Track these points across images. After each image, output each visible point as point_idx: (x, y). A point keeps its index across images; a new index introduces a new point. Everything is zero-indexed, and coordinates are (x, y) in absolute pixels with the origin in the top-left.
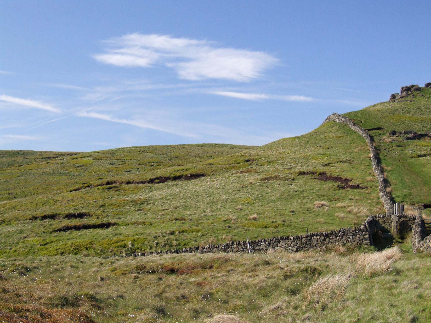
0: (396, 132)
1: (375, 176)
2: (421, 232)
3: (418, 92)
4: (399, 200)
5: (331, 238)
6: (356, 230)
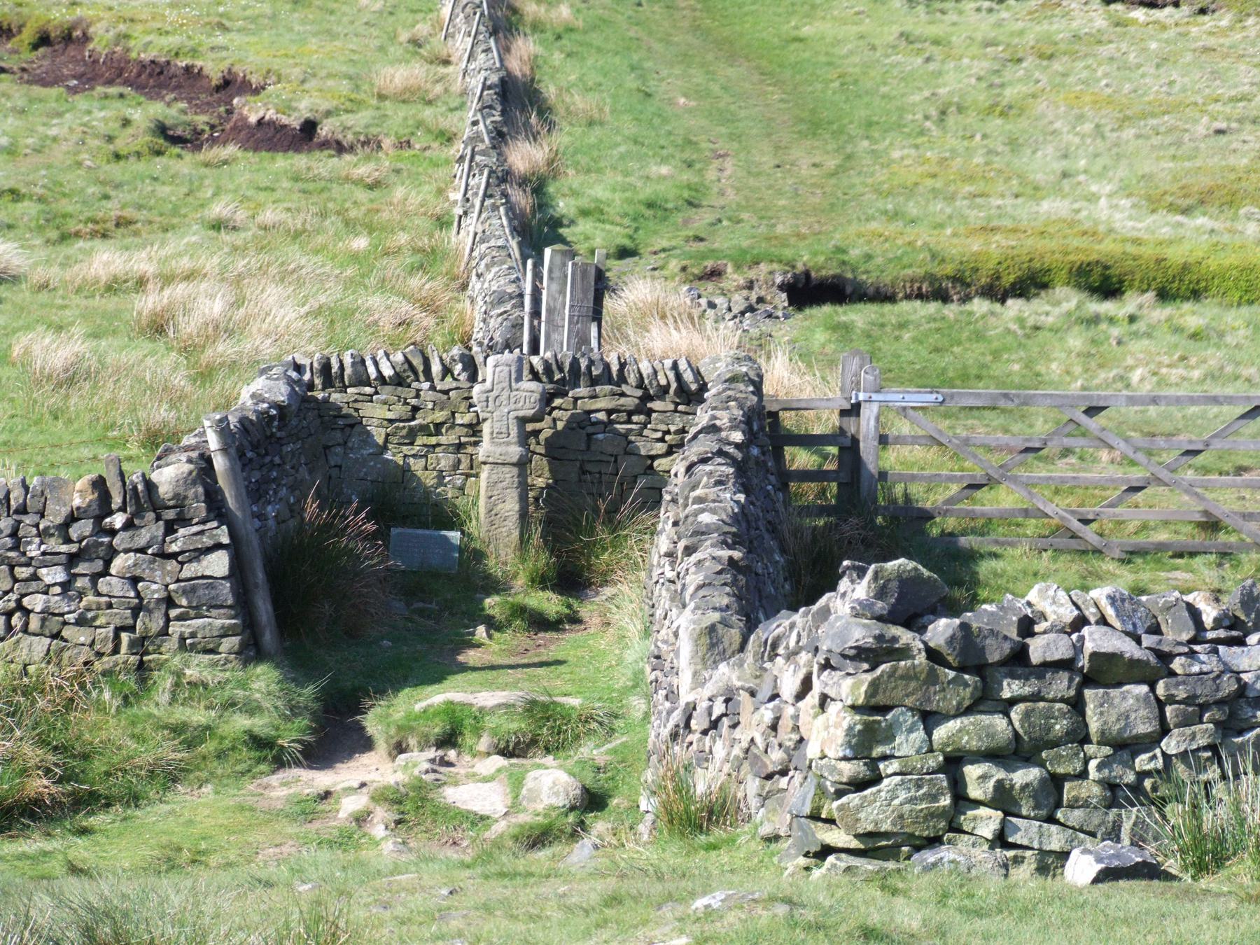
1: (446, 62)
2: (744, 529)
6: (104, 507)
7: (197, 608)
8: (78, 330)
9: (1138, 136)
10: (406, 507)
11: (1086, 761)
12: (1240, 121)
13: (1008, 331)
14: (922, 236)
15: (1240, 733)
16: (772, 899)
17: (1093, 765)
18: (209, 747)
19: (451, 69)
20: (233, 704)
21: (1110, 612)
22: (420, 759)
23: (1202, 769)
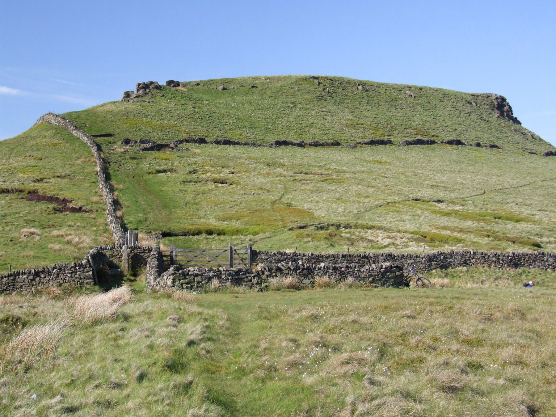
0: (130, 140)
2: (158, 266)
3: (158, 91)
4: (132, 227)
5: (43, 276)
6: (76, 266)
14: (182, 226)
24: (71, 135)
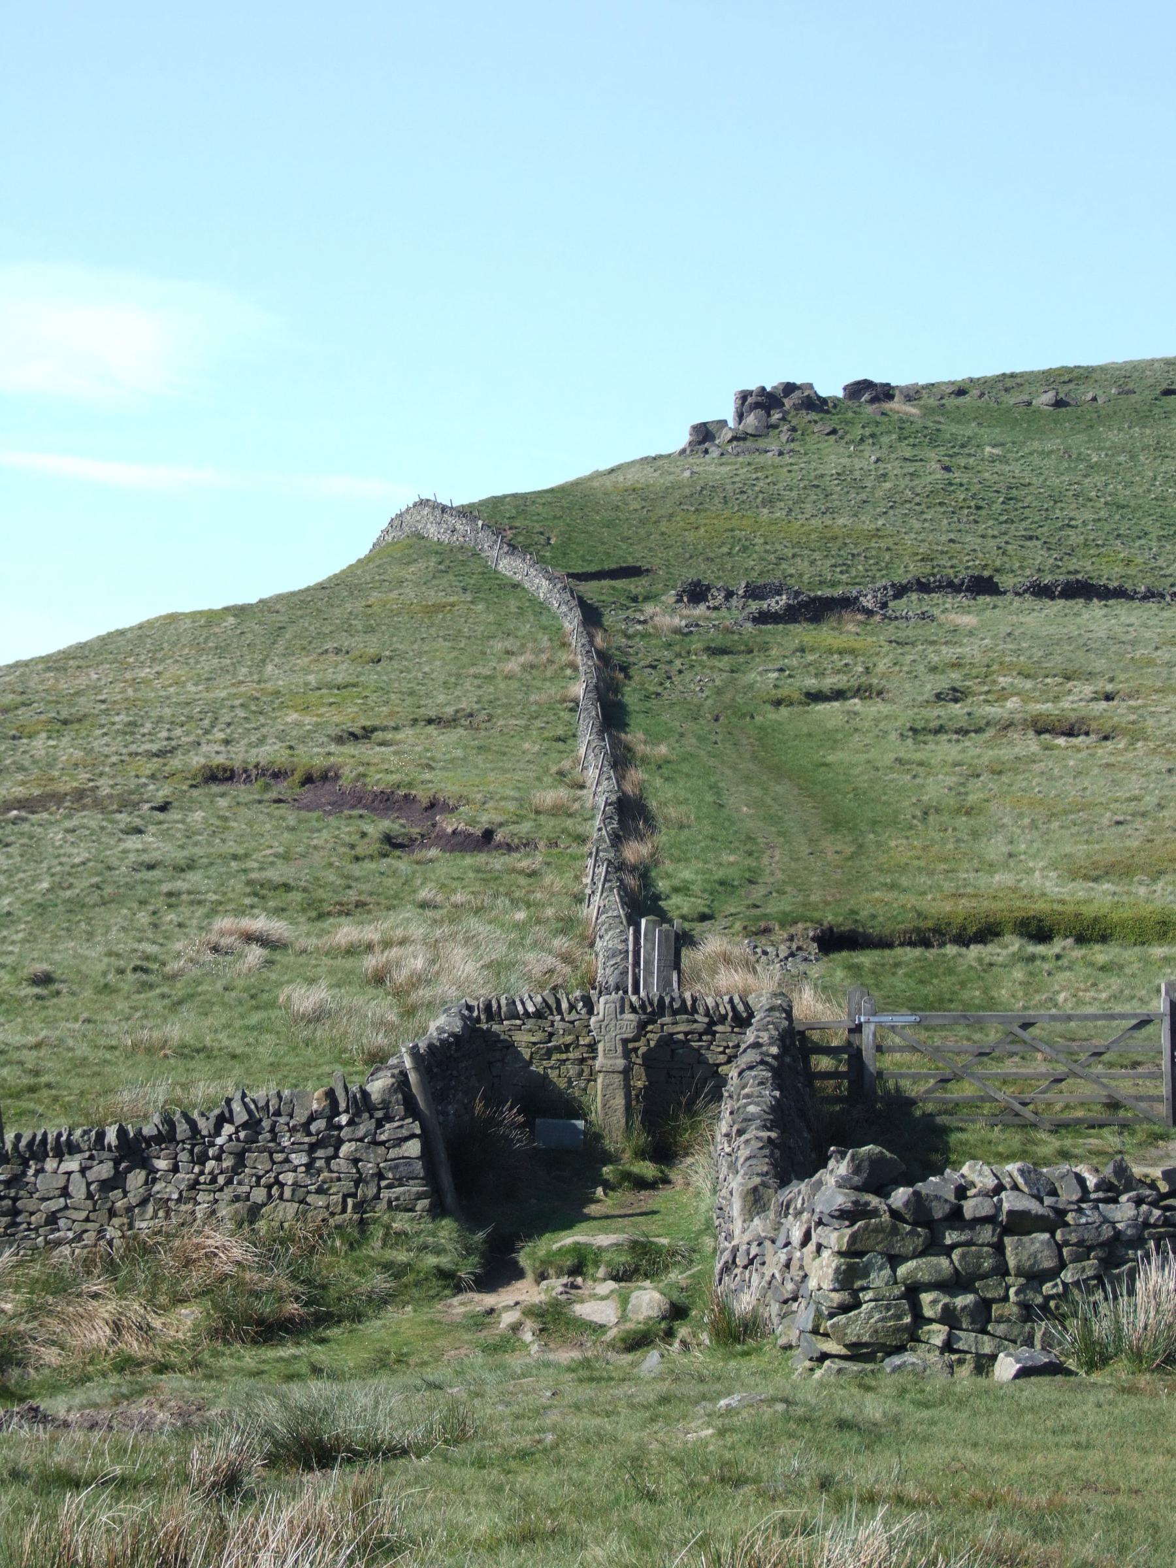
0: (708, 588)
1: (582, 787)
3: (813, 416)
4: (685, 911)
5: (162, 1164)
7: (400, 1179)
8: (323, 983)
9: (1062, 827)
10: (549, 1104)
11: (1007, 1288)
12: (1133, 815)
13: (971, 967)
14: (911, 900)
15: (1118, 1266)
16: (773, 1400)
17: (1012, 1291)
18: (409, 1278)
19: (585, 791)
20: (426, 1247)
21: (1020, 1181)
22: (557, 1284)
23: (1090, 1292)
24: (490, 575)
